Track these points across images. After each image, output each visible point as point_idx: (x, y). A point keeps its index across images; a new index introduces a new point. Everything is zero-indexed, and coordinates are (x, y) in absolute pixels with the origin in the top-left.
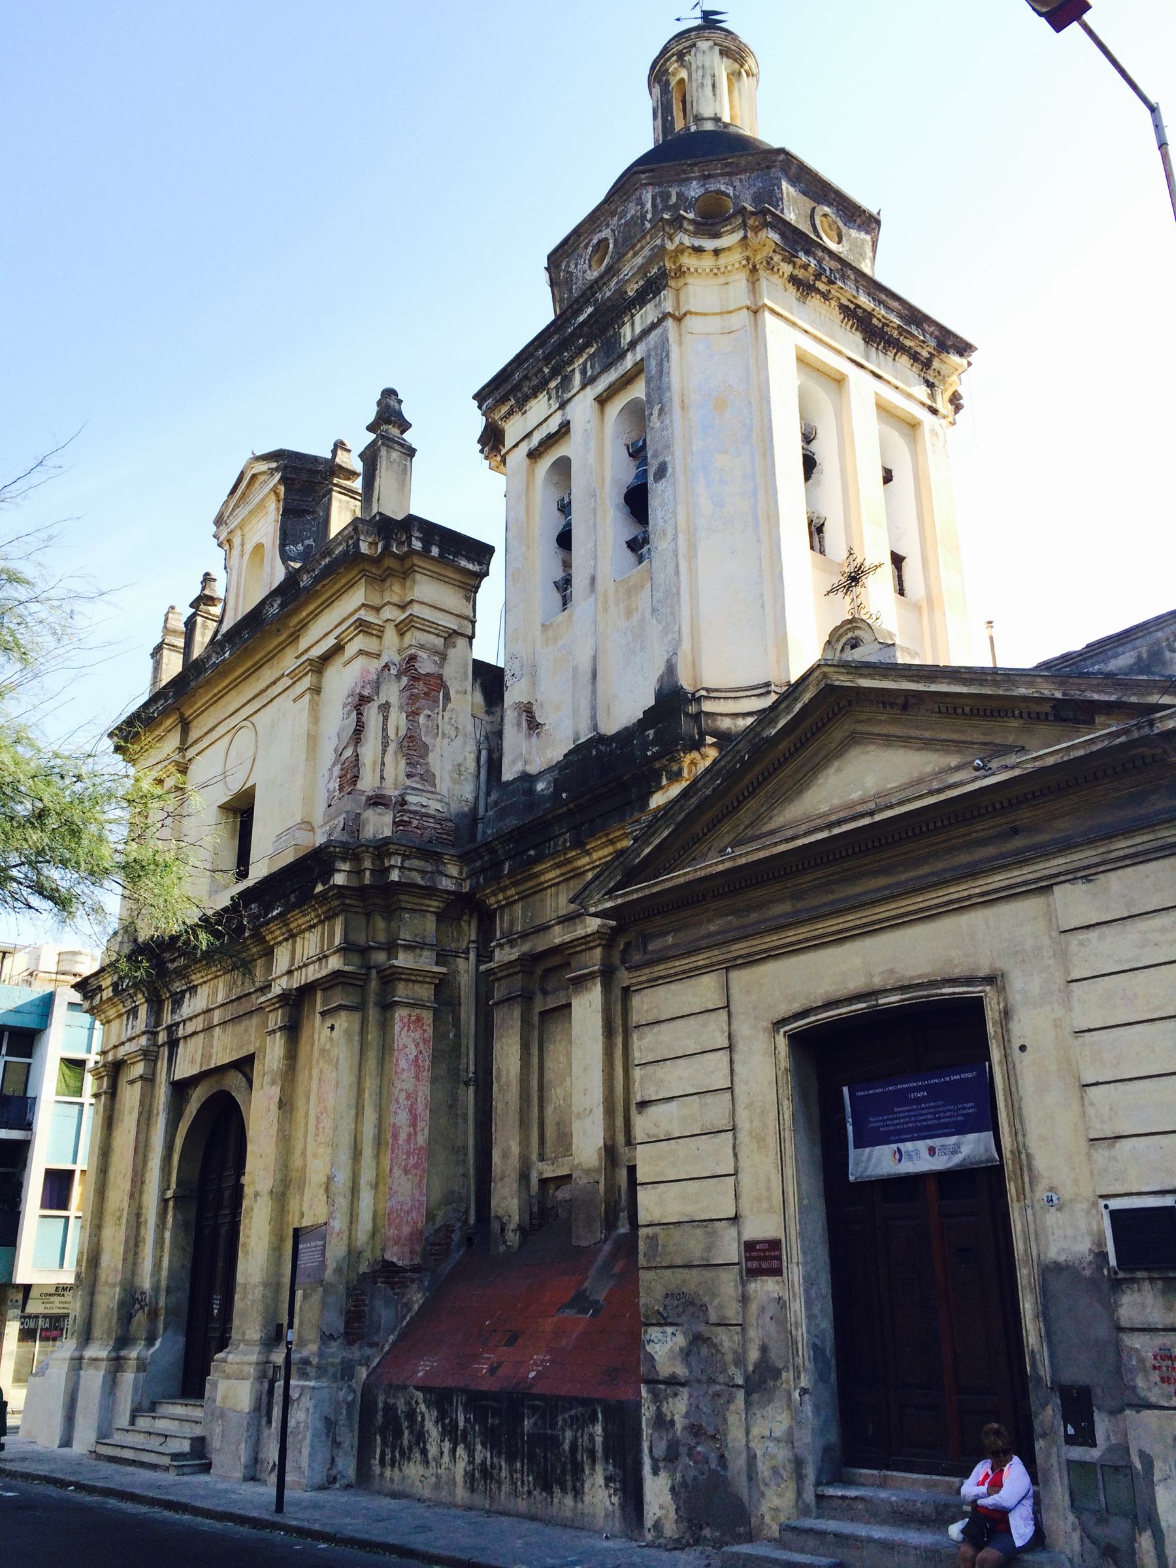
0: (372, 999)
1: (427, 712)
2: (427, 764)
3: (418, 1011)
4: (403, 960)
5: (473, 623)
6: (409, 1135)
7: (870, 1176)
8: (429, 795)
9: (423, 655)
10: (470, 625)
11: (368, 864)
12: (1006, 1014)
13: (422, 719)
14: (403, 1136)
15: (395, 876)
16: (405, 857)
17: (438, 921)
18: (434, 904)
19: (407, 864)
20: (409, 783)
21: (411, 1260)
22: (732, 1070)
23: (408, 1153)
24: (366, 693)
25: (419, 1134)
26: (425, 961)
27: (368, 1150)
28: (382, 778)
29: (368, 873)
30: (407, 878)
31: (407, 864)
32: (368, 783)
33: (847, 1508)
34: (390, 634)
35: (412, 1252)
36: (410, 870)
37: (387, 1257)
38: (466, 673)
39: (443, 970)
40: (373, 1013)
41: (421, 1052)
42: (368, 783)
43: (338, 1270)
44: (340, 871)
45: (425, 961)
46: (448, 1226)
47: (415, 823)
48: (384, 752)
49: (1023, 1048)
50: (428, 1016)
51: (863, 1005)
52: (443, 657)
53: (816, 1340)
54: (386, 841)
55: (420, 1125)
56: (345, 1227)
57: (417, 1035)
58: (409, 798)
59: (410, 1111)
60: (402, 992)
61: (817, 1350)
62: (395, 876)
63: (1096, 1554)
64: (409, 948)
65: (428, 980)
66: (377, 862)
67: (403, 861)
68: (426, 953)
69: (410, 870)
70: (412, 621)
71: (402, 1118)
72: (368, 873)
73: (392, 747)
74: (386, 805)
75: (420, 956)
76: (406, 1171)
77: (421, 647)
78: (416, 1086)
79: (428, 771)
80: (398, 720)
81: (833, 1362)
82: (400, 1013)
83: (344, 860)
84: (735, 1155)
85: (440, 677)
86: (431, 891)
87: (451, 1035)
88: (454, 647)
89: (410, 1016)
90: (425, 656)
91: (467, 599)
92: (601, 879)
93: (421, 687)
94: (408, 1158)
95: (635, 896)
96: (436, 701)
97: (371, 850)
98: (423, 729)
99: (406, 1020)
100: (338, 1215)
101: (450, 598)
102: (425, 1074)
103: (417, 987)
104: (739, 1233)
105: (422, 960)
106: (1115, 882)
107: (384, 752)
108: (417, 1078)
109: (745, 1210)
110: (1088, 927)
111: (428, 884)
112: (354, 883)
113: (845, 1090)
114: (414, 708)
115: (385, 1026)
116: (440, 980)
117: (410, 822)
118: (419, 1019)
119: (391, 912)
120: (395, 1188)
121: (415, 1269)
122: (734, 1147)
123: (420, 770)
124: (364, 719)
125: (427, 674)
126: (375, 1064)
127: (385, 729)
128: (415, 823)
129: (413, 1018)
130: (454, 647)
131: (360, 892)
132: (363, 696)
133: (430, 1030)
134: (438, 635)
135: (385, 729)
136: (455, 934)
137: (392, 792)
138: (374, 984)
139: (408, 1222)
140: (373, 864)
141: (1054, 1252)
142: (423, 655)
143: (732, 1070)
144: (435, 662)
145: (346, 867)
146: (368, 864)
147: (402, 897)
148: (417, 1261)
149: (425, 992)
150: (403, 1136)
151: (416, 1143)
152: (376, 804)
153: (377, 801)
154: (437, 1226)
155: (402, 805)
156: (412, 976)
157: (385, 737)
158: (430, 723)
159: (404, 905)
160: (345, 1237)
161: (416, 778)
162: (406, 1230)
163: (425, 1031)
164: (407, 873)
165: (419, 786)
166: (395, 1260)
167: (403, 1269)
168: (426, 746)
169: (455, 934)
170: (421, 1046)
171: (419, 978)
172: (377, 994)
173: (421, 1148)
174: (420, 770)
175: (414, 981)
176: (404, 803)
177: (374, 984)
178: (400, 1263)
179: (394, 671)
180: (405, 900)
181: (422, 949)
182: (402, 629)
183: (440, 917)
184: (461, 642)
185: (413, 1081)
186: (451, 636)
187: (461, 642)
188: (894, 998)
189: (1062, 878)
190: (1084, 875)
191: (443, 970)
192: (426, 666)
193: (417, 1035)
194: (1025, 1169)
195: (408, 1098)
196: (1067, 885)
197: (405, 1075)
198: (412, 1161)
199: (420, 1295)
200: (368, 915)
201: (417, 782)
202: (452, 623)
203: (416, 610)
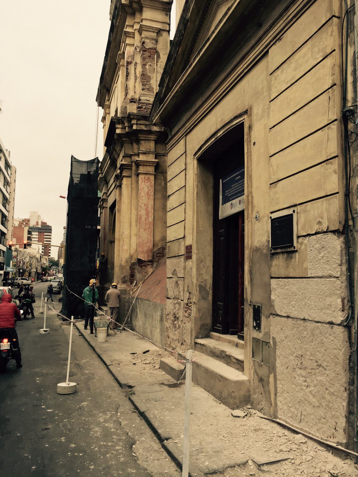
0: (133, 172)
1: (150, 63)
2: (150, 84)
3: (148, 176)
4: (142, 158)
5: (169, 25)
6: (146, 218)
7: (224, 217)
8: (150, 96)
9: (147, 41)
10: (168, 26)
11: (126, 124)
12: (250, 128)
13: (147, 67)
14: (143, 219)
15: (135, 127)
16: (138, 120)
17: (156, 144)
18: (153, 137)
19: (139, 122)
20: (143, 92)
21: (148, 258)
22: (186, 178)
23: (146, 224)
24: (129, 60)
25: (150, 218)
26: (151, 158)
27: (134, 223)
28: (135, 92)
29: (127, 128)
30: (140, 127)
31: (139, 122)
32: (131, 94)
33: (203, 348)
34: (137, 35)
35: (148, 256)
36: (140, 124)
37: (139, 257)
38: (167, 46)
39: (157, 160)
40: (134, 177)
41: (150, 190)
42: (131, 94)
43: (127, 262)
44: (118, 128)
45: (151, 158)
46: (163, 248)
47: (144, 107)
48: (135, 82)
49: (254, 144)
50: (152, 178)
51: (213, 139)
52: (157, 41)
53: (201, 284)
54: (133, 114)
55: (150, 214)
56: (128, 248)
57: (148, 184)
58: (141, 98)
59: (146, 210)
60: (142, 169)
61: (202, 288)
62: (135, 127)
63: (257, 381)
64: (144, 153)
65: (151, 165)
66: (130, 123)
67: (137, 122)
68: (151, 155)
69: (140, 124)
70: (142, 27)
71: (143, 212)
72: (127, 128)
73: (138, 80)
74: (135, 102)
75: (149, 156)
76: (145, 230)
77: (147, 38)
78: (148, 201)
79: (150, 87)
80: (139, 69)
81: (211, 292)
82: (141, 177)
83: (119, 124)
84: (185, 212)
85: (155, 49)
86: (150, 132)
87: (163, 184)
88: (162, 36)
89: (145, 177)
90: (148, 41)
91: (167, 15)
92: (154, 107)
93: (147, 54)
94: (146, 226)
95: (161, 111)
96: (154, 58)
97: (126, 119)
98: (148, 71)
99: (143, 179)
100: (126, 245)
101: (159, 16)
102: (152, 197)
103: (147, 167)
104: (185, 243)
105: (149, 158)
106: (289, 35)
107: (135, 82)
108: (148, 199)
109: (186, 235)
110: (278, 68)
111: (148, 129)
112: (124, 132)
113: (221, 180)
114: (144, 63)
115: (137, 182)
116: (156, 164)
117: (142, 107)
118: (148, 179)
119: (138, 142)
120: (141, 235)
121: (149, 261)
122: (185, 209)
123: (147, 87)
124: (129, 71)
125: (149, 49)
126: (135, 196)
127: (135, 73)
128: (144, 107)
129: (146, 178)
130: (162, 36)
131: (127, 135)
132: (128, 62)
133: (153, 182)
134: (154, 32)
135: (135, 73)
136: (164, 147)
137: (137, 97)
138: (134, 167)
139: (146, 246)
140: (128, 124)
141: (256, 244)
142: (147, 41)
143: (186, 178)
144: (153, 43)
145: (120, 126)
146: (126, 124)
147: (139, 135)
148: (150, 258)
149: (151, 169)
150: (143, 219)
151: (149, 221)
152: (131, 102)
153: (132, 101)
154: (159, 247)
155: (140, 101)
156: (146, 163)
157: (136, 76)
158: (151, 68)
159: (141, 138)
160: (128, 251)
161: (146, 90)
162: (145, 249)
163: (151, 182)
164: (139, 126)
165: (147, 93)
166: (141, 258)
167: (145, 261)
168: (149, 77)
169: (164, 147)
170: (150, 188)
171: (145, 164)
172: (135, 171)
173: (151, 222)
174: (147, 87)
175: (146, 165)
176: (140, 100)
177: (134, 167)
178: (143, 259)
179: (138, 50)
180: (141, 136)
181: (149, 153)
182: (140, 31)
183: (157, 142)
184: (165, 34)
185: (147, 200)
186: (159, 32)
187: (165, 34)
188: (221, 133)
189: (272, 43)
190: (278, 38)
191: (157, 160)
192: (149, 44)
193: (148, 184)
194: (250, 204)
195: (145, 205)
196: (274, 46)
197: (143, 198)
198: (147, 226)
199: (151, 270)
200: (132, 144)
201: (146, 92)
202: (159, 26)
203: (145, 23)
